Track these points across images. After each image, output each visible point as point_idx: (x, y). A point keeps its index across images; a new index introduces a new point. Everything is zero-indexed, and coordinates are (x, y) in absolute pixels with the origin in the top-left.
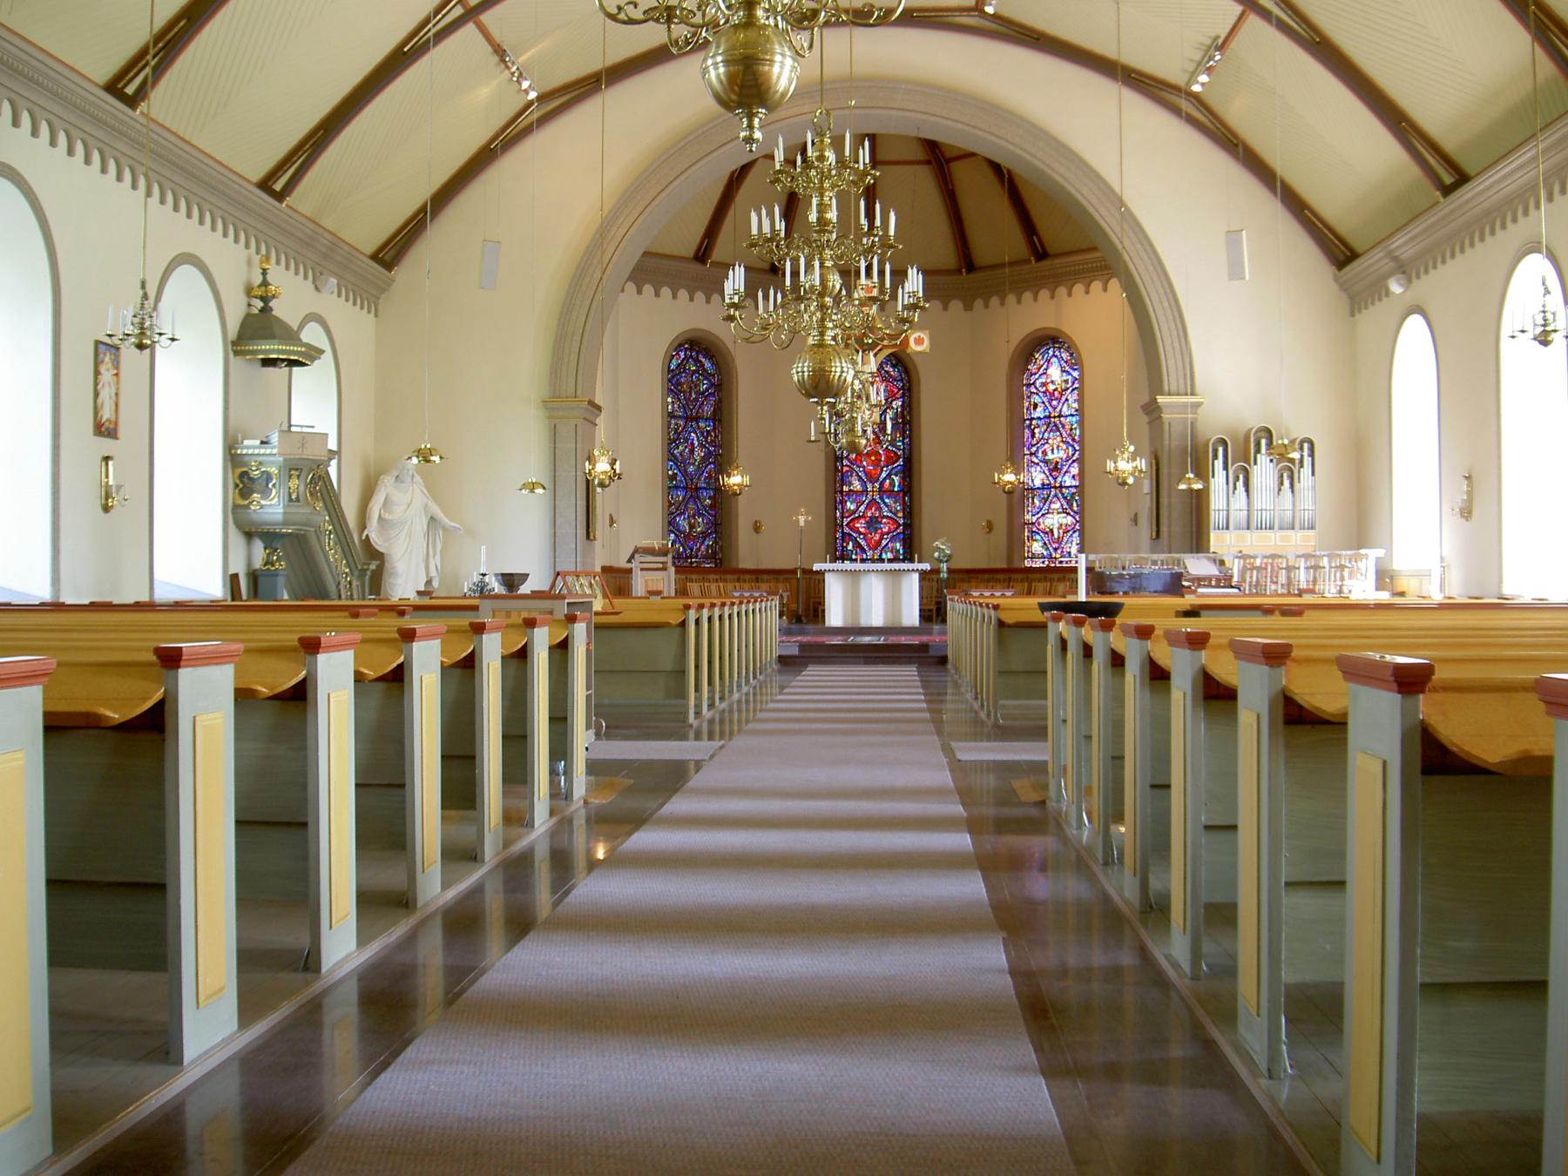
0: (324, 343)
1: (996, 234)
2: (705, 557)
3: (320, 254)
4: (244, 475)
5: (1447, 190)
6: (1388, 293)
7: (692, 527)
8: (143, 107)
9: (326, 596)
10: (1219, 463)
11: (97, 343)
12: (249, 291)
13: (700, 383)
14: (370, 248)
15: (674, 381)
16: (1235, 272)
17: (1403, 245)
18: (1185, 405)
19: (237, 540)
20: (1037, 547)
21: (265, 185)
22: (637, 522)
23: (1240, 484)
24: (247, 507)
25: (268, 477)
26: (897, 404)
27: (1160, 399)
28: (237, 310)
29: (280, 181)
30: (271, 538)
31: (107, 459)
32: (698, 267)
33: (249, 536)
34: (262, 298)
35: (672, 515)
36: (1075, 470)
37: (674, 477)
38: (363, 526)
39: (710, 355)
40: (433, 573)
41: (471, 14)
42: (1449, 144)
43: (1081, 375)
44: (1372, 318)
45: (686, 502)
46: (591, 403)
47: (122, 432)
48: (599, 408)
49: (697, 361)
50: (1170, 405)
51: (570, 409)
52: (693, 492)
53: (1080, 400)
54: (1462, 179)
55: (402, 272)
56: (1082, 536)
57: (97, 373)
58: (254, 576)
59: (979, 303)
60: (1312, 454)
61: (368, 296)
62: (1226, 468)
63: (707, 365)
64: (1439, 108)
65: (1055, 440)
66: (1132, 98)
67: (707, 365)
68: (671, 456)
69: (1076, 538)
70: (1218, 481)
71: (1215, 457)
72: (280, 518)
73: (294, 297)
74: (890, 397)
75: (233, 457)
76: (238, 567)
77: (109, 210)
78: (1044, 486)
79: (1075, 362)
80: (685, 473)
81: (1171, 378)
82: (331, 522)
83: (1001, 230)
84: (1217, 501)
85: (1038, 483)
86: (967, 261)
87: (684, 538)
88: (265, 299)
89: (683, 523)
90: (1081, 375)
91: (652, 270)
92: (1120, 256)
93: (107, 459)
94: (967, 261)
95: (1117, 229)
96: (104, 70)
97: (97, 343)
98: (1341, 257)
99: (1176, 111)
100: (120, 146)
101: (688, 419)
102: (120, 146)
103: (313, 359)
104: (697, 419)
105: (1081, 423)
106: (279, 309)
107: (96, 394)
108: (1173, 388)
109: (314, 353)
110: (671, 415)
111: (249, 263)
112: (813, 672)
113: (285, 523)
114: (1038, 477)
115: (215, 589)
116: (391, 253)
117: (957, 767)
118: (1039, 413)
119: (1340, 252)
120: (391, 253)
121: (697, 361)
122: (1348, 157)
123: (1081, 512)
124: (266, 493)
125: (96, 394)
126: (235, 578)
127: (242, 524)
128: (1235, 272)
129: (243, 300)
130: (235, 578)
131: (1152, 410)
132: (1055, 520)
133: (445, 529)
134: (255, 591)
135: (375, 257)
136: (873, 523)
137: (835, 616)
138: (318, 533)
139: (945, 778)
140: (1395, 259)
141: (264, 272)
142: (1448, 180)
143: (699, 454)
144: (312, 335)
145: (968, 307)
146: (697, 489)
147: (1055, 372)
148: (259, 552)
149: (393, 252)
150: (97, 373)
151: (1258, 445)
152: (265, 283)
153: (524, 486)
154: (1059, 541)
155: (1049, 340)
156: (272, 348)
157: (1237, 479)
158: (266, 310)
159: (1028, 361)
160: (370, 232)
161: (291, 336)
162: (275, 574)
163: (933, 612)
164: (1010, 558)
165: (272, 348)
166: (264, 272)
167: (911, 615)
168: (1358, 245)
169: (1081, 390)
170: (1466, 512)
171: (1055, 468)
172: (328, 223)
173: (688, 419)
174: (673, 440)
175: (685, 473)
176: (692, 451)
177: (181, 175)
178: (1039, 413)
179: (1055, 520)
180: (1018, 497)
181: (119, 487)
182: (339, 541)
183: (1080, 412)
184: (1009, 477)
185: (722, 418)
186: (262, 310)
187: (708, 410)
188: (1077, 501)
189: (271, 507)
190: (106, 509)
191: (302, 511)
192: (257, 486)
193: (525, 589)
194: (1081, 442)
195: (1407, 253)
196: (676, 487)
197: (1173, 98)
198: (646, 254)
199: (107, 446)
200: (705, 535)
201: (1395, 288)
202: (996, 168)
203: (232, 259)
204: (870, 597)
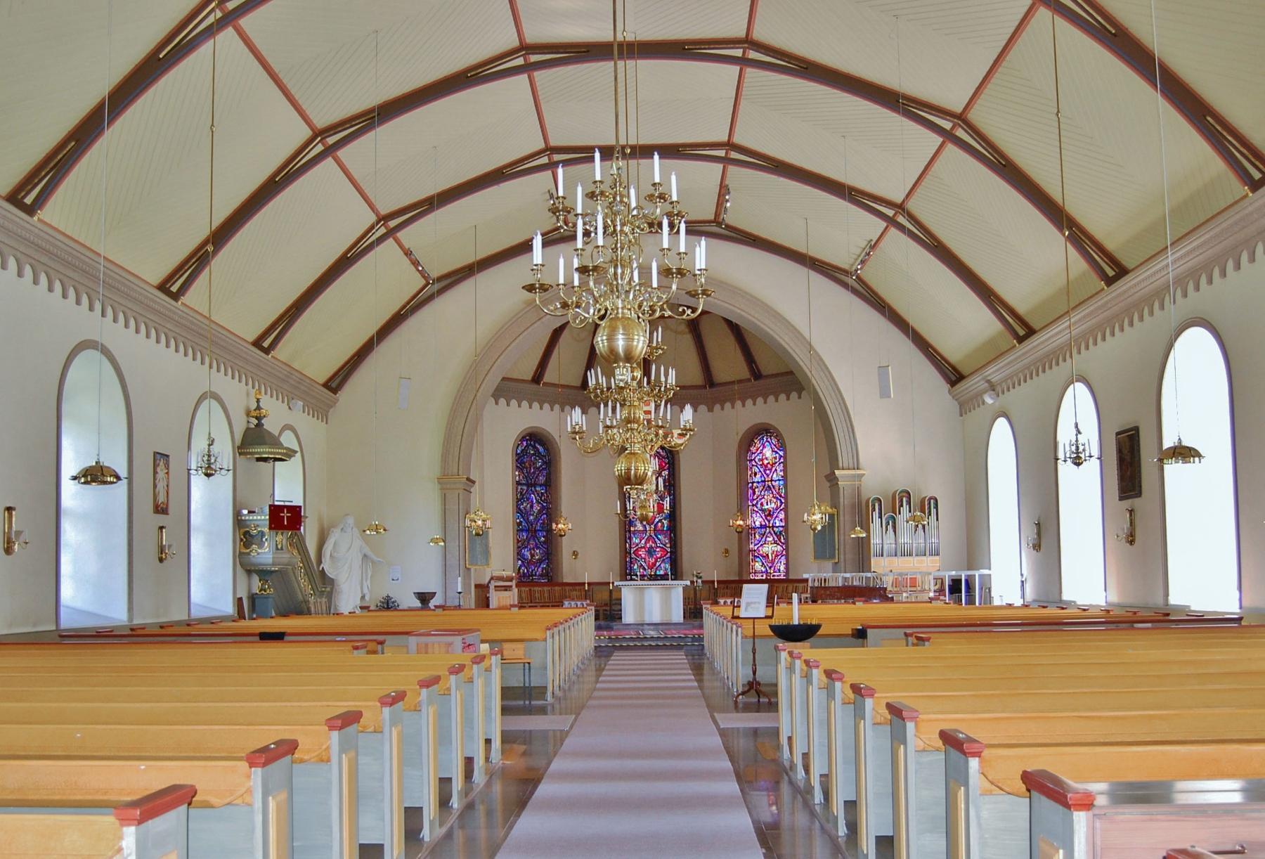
0: (297, 449)
1: (729, 365)
2: (541, 575)
3: (291, 386)
4: (247, 534)
5: (1021, 340)
6: (984, 402)
7: (532, 556)
8: (183, 299)
9: (300, 610)
10: (876, 514)
11: (155, 453)
12: (248, 414)
13: (536, 459)
14: (322, 380)
15: (521, 460)
16: (885, 393)
17: (994, 373)
18: (854, 476)
19: (241, 574)
20: (758, 566)
21: (257, 343)
22: (502, 558)
23: (890, 527)
24: (248, 554)
25: (263, 534)
26: (665, 473)
27: (837, 472)
28: (240, 426)
29: (266, 342)
30: (264, 574)
31: (161, 528)
32: (534, 386)
33: (249, 572)
34: (257, 418)
35: (520, 547)
36: (782, 516)
37: (520, 523)
38: (320, 562)
39: (543, 444)
40: (366, 591)
41: (230, 19)
42: (1021, 309)
43: (785, 453)
44: (975, 416)
45: (528, 539)
46: (468, 479)
47: (171, 510)
48: (474, 482)
49: (534, 447)
50: (843, 476)
51: (456, 484)
52: (533, 533)
53: (785, 470)
54: (1031, 332)
55: (345, 394)
56: (787, 559)
57: (155, 472)
58: (253, 598)
59: (717, 407)
60: (936, 507)
61: (321, 411)
62: (880, 517)
63: (541, 449)
64: (1020, 293)
65: (768, 496)
66: (816, 278)
67: (541, 449)
68: (519, 510)
69: (783, 560)
70: (875, 526)
71: (874, 509)
72: (270, 561)
73: (277, 415)
74: (662, 468)
75: (239, 522)
76: (243, 593)
77: (164, 366)
78: (762, 526)
79: (782, 446)
80: (527, 521)
81: (844, 457)
82: (302, 562)
83: (732, 363)
84: (875, 540)
85: (758, 524)
86: (709, 379)
87: (526, 563)
88: (259, 418)
89: (527, 554)
90: (785, 453)
91: (507, 389)
92: (810, 381)
93: (161, 528)
94: (709, 379)
95: (808, 363)
96: (156, 277)
97: (155, 453)
98: (954, 378)
99: (845, 285)
100: (168, 326)
101: (532, 485)
102: (168, 326)
103: (290, 457)
104: (535, 485)
105: (785, 486)
106: (268, 424)
107: (155, 486)
108: (846, 465)
109: (290, 454)
110: (518, 483)
111: (248, 394)
112: (618, 657)
113: (274, 564)
114: (758, 521)
115: (229, 608)
116: (336, 383)
117: (723, 733)
118: (758, 478)
119: (954, 376)
120: (336, 383)
121: (534, 447)
122: (962, 323)
123: (786, 543)
124: (261, 545)
125: (155, 486)
126: (240, 599)
127: (245, 565)
128: (885, 393)
129: (244, 418)
130: (240, 599)
131: (832, 479)
132: (769, 548)
133: (373, 562)
134: (253, 607)
135: (326, 385)
136: (650, 552)
137: (629, 616)
138: (294, 569)
139: (717, 741)
140: (988, 381)
141: (258, 401)
142: (1021, 332)
143: (537, 508)
144: (288, 440)
145: (711, 410)
146: (536, 531)
147: (768, 453)
148: (256, 584)
149: (337, 381)
150: (155, 472)
151: (901, 501)
152: (259, 408)
153: (432, 540)
154: (773, 561)
155: (762, 431)
156: (264, 451)
157: (888, 523)
158: (259, 425)
159: (750, 446)
160: (321, 370)
161: (276, 442)
162: (267, 597)
163: (693, 612)
164: (740, 573)
165: (264, 451)
166: (258, 401)
167: (677, 615)
168: (965, 371)
169: (785, 464)
170: (1037, 547)
171: (769, 514)
172: (296, 365)
173: (528, 485)
174: (520, 499)
175: (527, 521)
176: (532, 507)
177: (204, 341)
178: (758, 478)
179: (769, 548)
180: (745, 534)
181: (170, 546)
182: (306, 573)
183: (785, 478)
184: (741, 523)
185: (551, 484)
186: (257, 425)
187: (542, 479)
188: (783, 536)
189: (265, 554)
190: (161, 560)
191: (285, 557)
192: (255, 540)
193: (432, 604)
194: (786, 498)
195: (995, 378)
196: (522, 530)
197: (843, 278)
198: (504, 379)
199: (161, 519)
200: (540, 561)
201: (989, 400)
202: (729, 323)
203: (237, 393)
204: (652, 604)
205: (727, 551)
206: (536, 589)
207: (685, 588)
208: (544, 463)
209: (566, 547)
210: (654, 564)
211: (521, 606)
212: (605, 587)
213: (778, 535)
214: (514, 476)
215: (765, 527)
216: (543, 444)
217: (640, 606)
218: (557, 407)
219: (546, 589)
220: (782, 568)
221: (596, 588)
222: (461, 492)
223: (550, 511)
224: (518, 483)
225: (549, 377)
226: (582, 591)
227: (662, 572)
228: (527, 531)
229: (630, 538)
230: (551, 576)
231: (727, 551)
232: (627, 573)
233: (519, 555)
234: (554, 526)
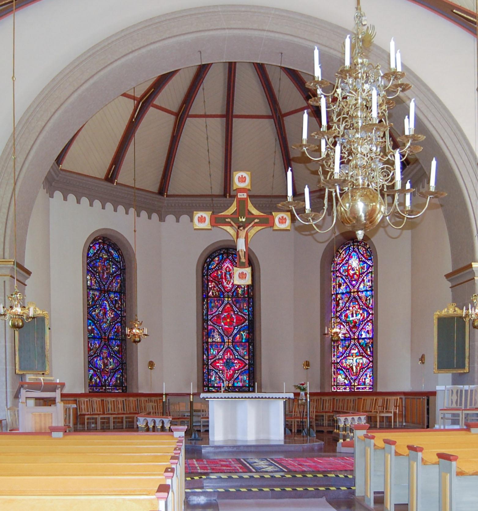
2: (115, 386)
7: (105, 365)
13: (109, 267)
15: (91, 265)
20: (341, 378)
36: (369, 327)
37: (92, 331)
39: (117, 250)
48: (29, 273)
49: (108, 252)
52: (107, 342)
65: (354, 307)
69: (369, 373)
78: (345, 339)
101: (105, 291)
104: (109, 292)
136: (228, 364)
143: (110, 315)
146: (109, 339)
147: (354, 263)
154: (357, 374)
164: (322, 385)
171: (355, 326)
174: (91, 306)
176: (105, 314)
187: (116, 286)
196: (94, 337)
200: (114, 371)
205: (307, 364)
206: (110, 399)
207: (288, 403)
208: (118, 269)
209: (142, 354)
210: (232, 376)
211: (66, 431)
212: (188, 397)
213: (364, 347)
214: (85, 281)
215: (350, 339)
216: (117, 250)
217: (231, 424)
218: (132, 211)
219: (120, 399)
220: (368, 381)
221: (172, 399)
222: (7, 278)
223: (123, 318)
224: (89, 288)
225: (125, 176)
226: (160, 403)
227: (240, 384)
228: (100, 338)
229: (208, 350)
230: (123, 388)
231: (307, 364)
232: (206, 385)
233: (91, 364)
234: (128, 331)
